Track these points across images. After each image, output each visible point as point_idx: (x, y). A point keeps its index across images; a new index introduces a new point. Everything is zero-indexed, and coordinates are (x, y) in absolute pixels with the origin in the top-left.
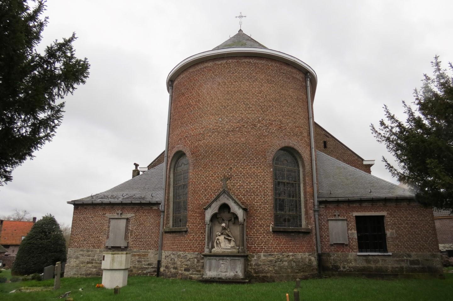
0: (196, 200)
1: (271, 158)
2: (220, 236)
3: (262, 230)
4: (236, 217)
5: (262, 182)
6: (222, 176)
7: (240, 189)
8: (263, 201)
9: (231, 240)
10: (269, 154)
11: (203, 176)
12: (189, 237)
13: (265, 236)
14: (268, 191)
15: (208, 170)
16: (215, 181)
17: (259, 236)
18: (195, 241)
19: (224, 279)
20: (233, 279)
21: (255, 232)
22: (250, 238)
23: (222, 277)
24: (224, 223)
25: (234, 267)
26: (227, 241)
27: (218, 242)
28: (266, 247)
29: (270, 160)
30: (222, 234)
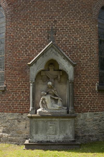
0: (14, 56)
1: (96, 13)
2: (45, 95)
3: (88, 89)
4: (64, 73)
5: (88, 38)
6: (46, 29)
7: (66, 44)
8: (89, 58)
9: (58, 99)
10: (95, 8)
11: (23, 29)
12: (8, 97)
13: (91, 95)
14: (93, 48)
15: (29, 23)
16: (38, 35)
17: (85, 95)
18: (14, 101)
19: (53, 142)
20: (63, 142)
21: (81, 91)
22: (76, 98)
23: (51, 140)
24: (50, 81)
25: (63, 128)
26: (53, 101)
27: (44, 102)
28: (92, 106)
29: (95, 15)
30: (48, 93)
